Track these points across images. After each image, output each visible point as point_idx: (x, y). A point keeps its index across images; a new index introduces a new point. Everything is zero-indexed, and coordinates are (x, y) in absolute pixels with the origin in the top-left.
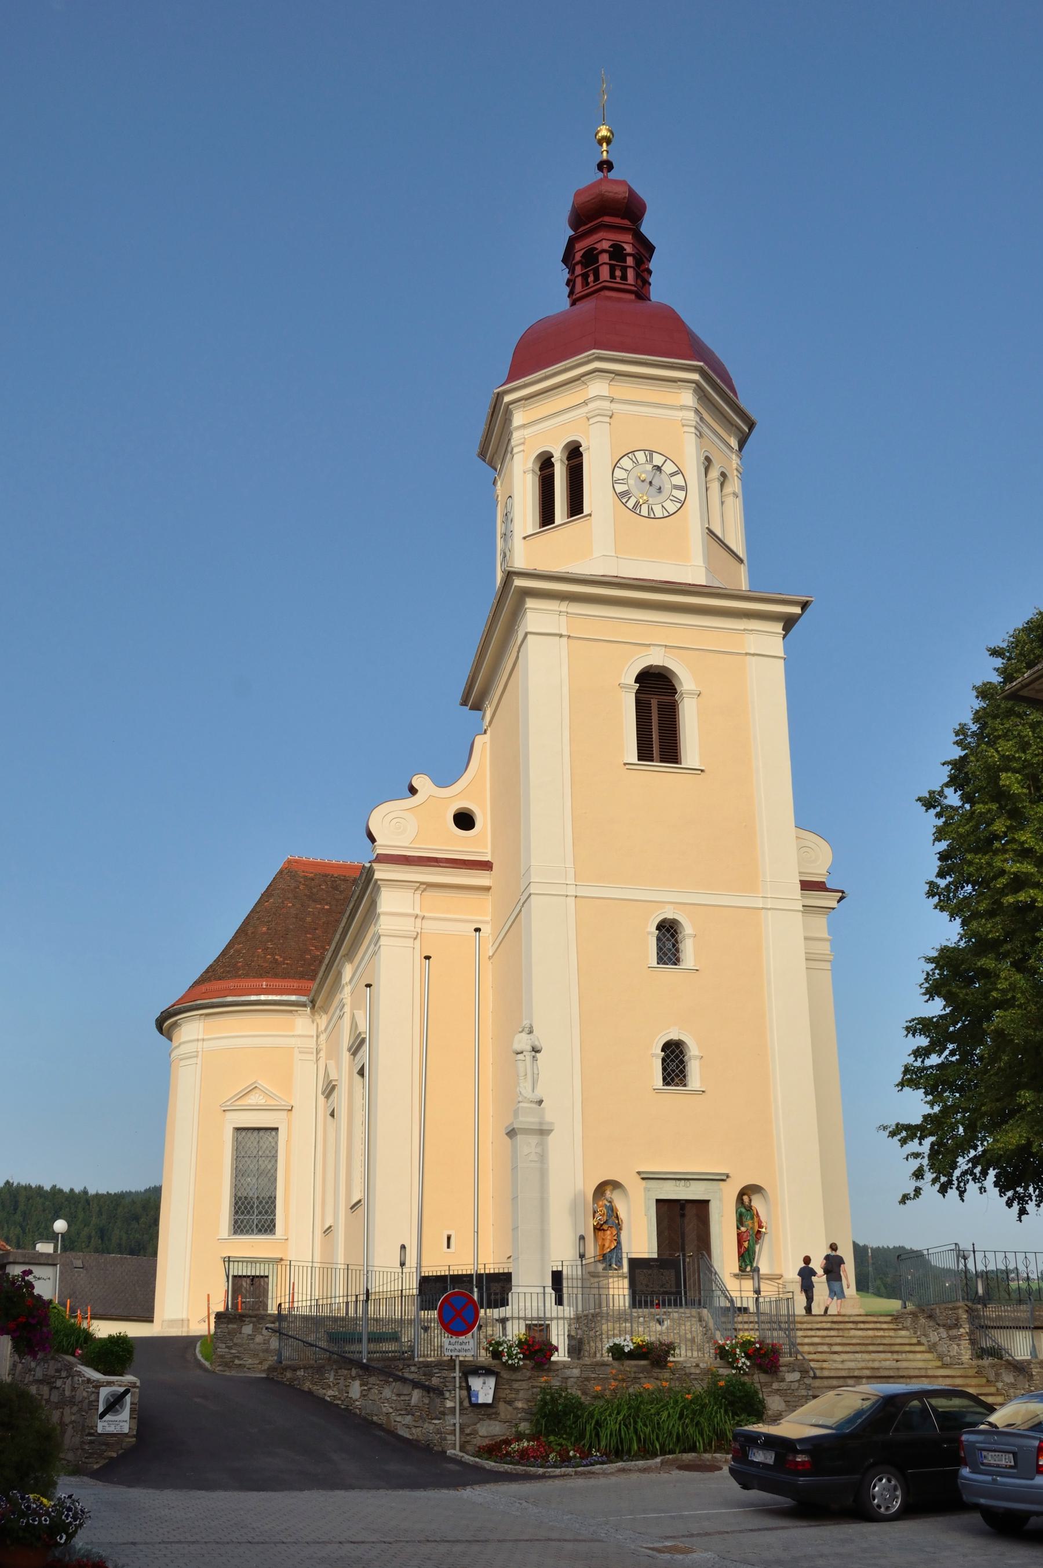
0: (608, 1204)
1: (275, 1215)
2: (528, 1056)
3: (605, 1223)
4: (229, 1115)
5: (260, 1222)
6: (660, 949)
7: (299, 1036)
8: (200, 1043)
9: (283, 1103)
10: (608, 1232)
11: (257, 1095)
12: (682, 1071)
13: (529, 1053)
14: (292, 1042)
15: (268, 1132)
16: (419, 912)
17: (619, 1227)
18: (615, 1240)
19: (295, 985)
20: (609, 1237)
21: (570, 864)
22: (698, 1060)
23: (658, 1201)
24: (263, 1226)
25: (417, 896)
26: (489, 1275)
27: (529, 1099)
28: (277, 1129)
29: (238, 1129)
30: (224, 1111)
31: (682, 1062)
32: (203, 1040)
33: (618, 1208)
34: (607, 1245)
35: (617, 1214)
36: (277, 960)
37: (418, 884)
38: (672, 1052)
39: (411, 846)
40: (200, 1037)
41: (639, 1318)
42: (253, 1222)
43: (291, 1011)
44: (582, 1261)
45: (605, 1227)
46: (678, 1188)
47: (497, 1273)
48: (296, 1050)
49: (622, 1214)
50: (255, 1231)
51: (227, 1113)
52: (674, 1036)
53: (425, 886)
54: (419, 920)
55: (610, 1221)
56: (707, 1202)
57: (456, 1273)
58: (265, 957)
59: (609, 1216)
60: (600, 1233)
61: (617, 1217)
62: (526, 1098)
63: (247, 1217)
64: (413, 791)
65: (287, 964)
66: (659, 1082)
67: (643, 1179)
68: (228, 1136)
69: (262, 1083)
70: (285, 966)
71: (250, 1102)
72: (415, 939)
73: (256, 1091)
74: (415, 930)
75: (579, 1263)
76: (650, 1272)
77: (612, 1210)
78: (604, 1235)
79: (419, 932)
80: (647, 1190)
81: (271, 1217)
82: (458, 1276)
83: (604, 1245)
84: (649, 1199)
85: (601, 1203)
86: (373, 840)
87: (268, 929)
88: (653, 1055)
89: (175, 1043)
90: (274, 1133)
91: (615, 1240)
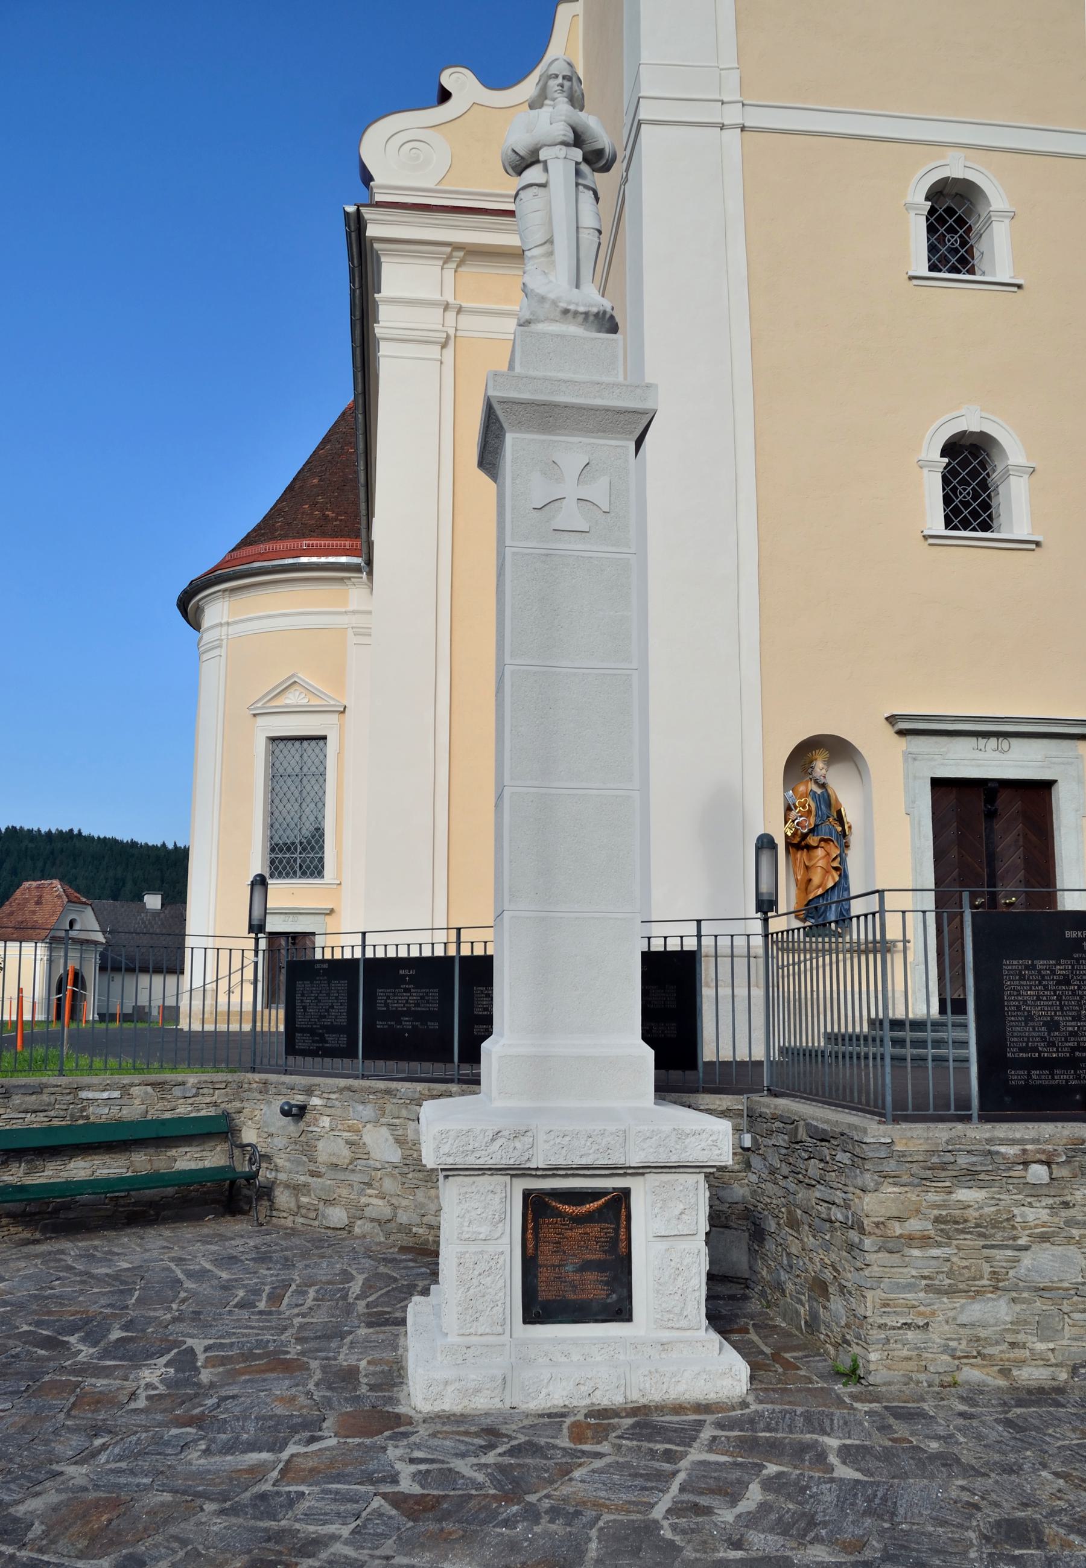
0: (819, 791)
1: (323, 853)
2: (591, 298)
3: (812, 831)
4: (260, 720)
5: (304, 860)
6: (932, 249)
7: (354, 612)
8: (224, 629)
9: (332, 703)
10: (820, 852)
11: (297, 693)
12: (986, 506)
13: (562, 151)
14: (344, 620)
15: (313, 743)
16: (451, 300)
17: (843, 838)
18: (836, 869)
19: (347, 543)
20: (821, 863)
21: (729, 59)
22: (1026, 476)
23: (937, 783)
24: (308, 867)
25: (449, 274)
26: (373, 964)
27: (554, 303)
28: (324, 738)
29: (273, 739)
30: (255, 715)
31: (984, 485)
32: (228, 624)
33: (841, 800)
34: (816, 879)
35: (839, 812)
36: (328, 516)
37: (448, 249)
38: (964, 464)
39: (438, 187)
40: (224, 620)
41: (1026, 1164)
42: (295, 860)
43: (342, 579)
44: (766, 921)
45: (812, 840)
46: (981, 755)
47: (338, 961)
48: (350, 632)
49: (850, 815)
50: (299, 873)
51: (259, 719)
52: (971, 422)
53: (461, 254)
54: (451, 315)
55: (824, 829)
56: (1047, 786)
57: (380, 954)
58: (312, 513)
59: (822, 818)
60: (802, 855)
61: (840, 819)
62: (542, 299)
63: (288, 856)
64: (445, 96)
65: (341, 520)
66: (936, 523)
67: (902, 733)
68: (260, 747)
69: (303, 676)
70: (338, 523)
71: (288, 702)
72: (444, 346)
73: (296, 687)
74: (445, 329)
75: (757, 926)
76: (1062, 969)
77: (829, 805)
78: (810, 859)
79: (452, 332)
80: (911, 757)
81: (319, 856)
82: (386, 961)
83: (810, 880)
84: (915, 778)
85: (802, 788)
86: (367, 178)
87: (320, 480)
88: (922, 464)
89: (208, 637)
90: (321, 743)
91: (836, 869)
